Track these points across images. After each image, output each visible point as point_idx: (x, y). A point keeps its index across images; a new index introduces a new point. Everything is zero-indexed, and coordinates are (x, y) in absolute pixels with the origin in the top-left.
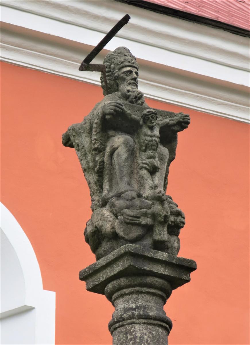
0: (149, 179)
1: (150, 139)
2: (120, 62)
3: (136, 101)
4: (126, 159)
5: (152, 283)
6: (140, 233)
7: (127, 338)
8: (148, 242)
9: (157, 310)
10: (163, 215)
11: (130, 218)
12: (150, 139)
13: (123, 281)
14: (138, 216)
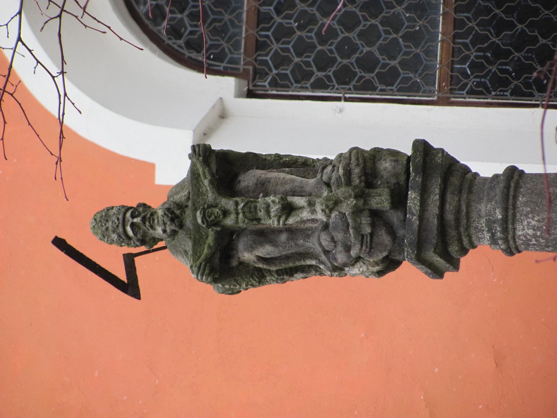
0: (300, 215)
1: (241, 216)
2: (119, 239)
3: (177, 217)
4: (272, 246)
5: (454, 211)
6: (384, 232)
7: (534, 245)
8: (395, 217)
9: (491, 202)
10: (355, 202)
11: (364, 248)
12: (241, 216)
14: (360, 238)
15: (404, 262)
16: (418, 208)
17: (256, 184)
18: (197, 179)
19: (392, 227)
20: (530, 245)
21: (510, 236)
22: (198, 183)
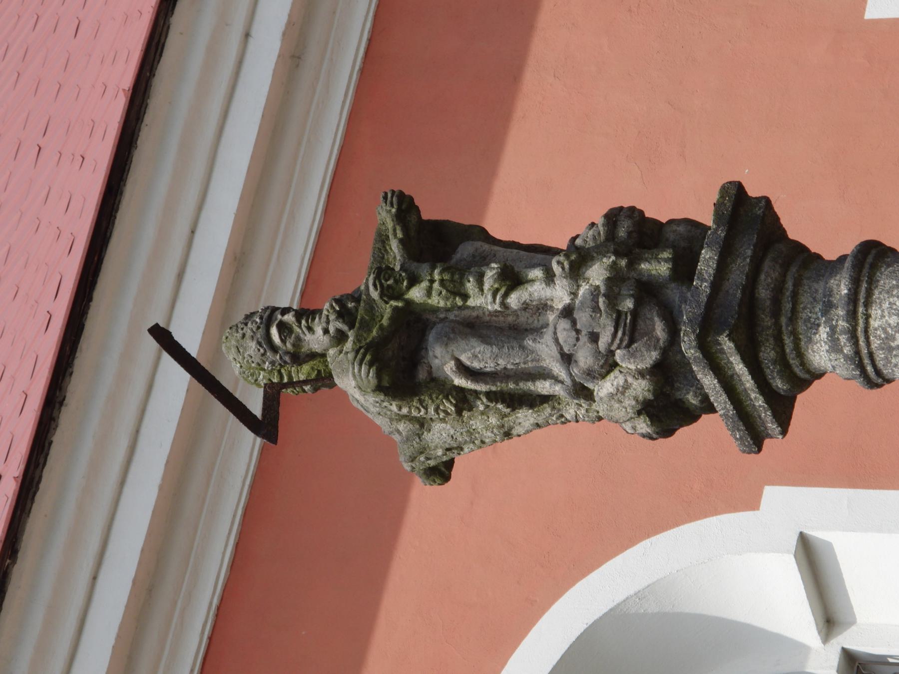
8: (673, 293)
13: (767, 354)
15: (706, 419)
16: (711, 271)
17: (474, 256)
18: (383, 242)
19: (671, 313)
20: (894, 349)
21: (859, 329)
22: (384, 247)
